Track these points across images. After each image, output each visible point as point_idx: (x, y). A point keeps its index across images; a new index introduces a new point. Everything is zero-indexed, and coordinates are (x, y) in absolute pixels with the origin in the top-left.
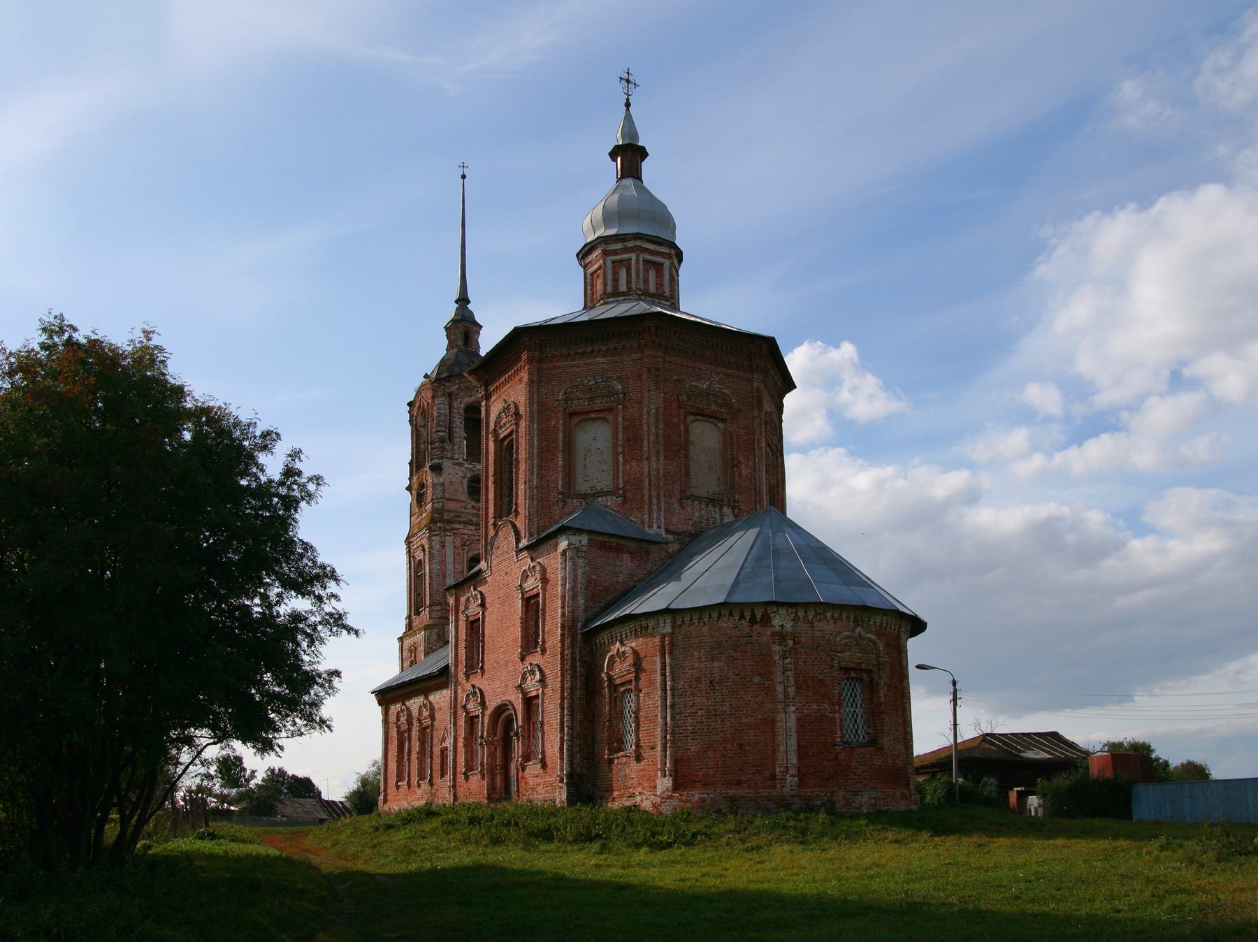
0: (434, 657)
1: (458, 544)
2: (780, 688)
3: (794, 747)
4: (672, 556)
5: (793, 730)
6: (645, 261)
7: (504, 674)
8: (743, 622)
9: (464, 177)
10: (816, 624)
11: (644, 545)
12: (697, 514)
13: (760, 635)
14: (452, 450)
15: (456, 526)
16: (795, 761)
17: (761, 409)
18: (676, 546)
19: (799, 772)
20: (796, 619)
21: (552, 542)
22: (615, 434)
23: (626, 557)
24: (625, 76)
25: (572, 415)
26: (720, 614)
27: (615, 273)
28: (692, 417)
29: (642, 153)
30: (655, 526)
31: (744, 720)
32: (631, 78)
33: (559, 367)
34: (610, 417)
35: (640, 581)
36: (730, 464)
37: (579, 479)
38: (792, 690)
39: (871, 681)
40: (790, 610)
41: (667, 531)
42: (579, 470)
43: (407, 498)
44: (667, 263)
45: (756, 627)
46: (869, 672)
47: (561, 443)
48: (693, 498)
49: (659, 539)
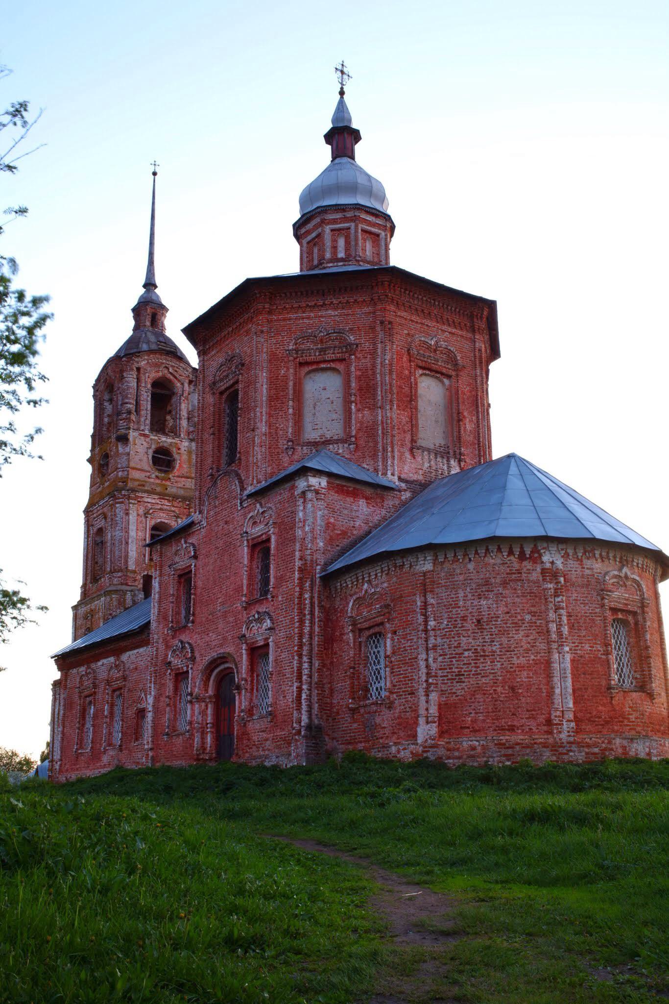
1: (141, 512)
2: (553, 627)
3: (570, 690)
4: (404, 504)
5: (569, 671)
6: (363, 231)
8: (512, 558)
9: (155, 174)
10: (585, 561)
12: (427, 465)
13: (529, 572)
15: (140, 494)
16: (571, 705)
18: (408, 495)
19: (575, 717)
20: (566, 556)
21: (288, 485)
23: (362, 502)
24: (340, 67)
25: (301, 364)
26: (487, 550)
27: (335, 241)
28: (421, 372)
30: (389, 473)
32: (345, 70)
33: (290, 319)
34: (341, 367)
35: (376, 526)
37: (308, 426)
38: (565, 630)
39: (636, 624)
40: (560, 547)
41: (400, 479)
42: (308, 419)
43: (88, 469)
45: (525, 563)
46: (634, 614)
47: (291, 392)
48: (423, 449)
49: (393, 486)
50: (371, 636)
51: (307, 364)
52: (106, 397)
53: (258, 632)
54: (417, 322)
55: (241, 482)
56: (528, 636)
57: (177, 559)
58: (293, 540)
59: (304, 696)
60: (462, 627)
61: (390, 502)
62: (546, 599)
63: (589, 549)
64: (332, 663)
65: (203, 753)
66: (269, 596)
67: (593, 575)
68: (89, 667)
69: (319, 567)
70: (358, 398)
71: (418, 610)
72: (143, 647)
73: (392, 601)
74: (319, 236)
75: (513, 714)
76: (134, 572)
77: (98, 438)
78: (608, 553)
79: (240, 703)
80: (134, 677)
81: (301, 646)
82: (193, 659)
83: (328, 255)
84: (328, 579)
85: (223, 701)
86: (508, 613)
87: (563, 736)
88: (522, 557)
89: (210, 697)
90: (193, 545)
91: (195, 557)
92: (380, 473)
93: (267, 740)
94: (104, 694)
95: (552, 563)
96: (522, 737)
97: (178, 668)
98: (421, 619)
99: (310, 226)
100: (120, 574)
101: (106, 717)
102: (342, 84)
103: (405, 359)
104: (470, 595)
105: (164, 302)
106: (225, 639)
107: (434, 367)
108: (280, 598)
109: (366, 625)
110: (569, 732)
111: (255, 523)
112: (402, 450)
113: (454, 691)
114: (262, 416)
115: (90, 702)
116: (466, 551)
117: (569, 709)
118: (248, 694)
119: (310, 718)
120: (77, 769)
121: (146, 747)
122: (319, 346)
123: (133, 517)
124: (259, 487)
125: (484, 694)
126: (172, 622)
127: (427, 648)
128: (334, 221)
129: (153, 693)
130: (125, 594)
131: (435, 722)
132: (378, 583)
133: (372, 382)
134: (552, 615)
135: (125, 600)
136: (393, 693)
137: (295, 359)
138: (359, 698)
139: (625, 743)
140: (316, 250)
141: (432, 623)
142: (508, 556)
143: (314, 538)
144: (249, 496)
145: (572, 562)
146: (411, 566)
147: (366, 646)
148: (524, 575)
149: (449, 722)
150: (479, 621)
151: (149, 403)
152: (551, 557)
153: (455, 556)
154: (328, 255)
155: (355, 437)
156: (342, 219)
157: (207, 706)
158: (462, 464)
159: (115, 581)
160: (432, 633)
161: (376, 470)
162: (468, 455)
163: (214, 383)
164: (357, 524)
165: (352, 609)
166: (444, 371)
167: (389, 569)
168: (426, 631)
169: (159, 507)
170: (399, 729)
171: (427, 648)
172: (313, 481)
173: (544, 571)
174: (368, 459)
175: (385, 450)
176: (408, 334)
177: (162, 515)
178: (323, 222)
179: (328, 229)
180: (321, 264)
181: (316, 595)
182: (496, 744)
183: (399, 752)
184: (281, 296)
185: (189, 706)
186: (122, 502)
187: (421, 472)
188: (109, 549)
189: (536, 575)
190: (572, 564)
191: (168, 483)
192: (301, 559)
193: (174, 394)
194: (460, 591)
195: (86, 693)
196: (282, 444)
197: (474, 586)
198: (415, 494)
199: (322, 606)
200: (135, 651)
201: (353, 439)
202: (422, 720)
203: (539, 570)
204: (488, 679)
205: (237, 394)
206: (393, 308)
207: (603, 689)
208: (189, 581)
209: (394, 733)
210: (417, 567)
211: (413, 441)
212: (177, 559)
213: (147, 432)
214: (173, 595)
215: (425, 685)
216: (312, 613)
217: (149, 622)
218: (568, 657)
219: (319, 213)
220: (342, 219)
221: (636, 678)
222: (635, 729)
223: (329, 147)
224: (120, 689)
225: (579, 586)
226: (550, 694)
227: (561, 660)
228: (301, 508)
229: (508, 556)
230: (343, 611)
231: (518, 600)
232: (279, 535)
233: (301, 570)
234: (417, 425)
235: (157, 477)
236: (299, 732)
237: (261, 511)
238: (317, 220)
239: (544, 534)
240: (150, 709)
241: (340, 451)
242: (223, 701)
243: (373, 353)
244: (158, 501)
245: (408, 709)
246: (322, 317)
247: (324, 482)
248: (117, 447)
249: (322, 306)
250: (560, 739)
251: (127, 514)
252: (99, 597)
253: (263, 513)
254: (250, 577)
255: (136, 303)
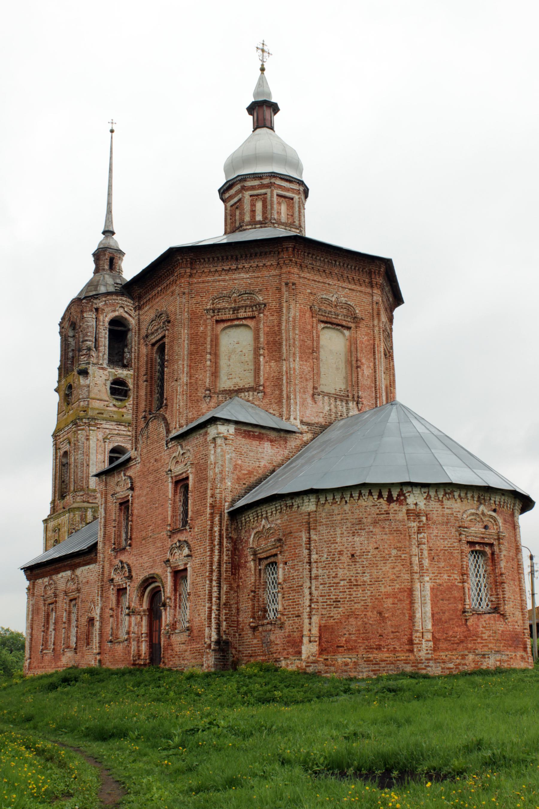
0: (76, 537)
1: (100, 437)
2: (415, 560)
3: (429, 614)
4: (306, 444)
6: (278, 195)
7: (152, 550)
9: (112, 131)
10: (445, 502)
11: (282, 434)
12: (327, 408)
14: (98, 357)
15: (99, 422)
16: (430, 627)
17: (379, 320)
19: (433, 637)
20: (428, 498)
21: (202, 431)
22: (257, 338)
23: (267, 445)
24: (261, 46)
25: (218, 322)
26: (360, 494)
27: (253, 205)
28: (323, 325)
29: (275, 108)
31: (383, 589)
32: (266, 48)
33: (208, 282)
35: (279, 465)
36: (353, 365)
38: (426, 562)
39: (493, 554)
41: (302, 422)
43: (56, 397)
44: (296, 197)
45: (393, 505)
46: (491, 545)
50: (268, 565)
51: (223, 321)
52: (71, 334)
53: (179, 559)
54: (319, 282)
55: (167, 425)
56: (394, 568)
57: (118, 489)
58: (206, 479)
59: (213, 615)
60: (339, 560)
61: (293, 443)
62: (410, 536)
63: (449, 491)
64: (238, 586)
65: (139, 659)
66: (187, 528)
67: (452, 514)
68: (51, 579)
69: (227, 504)
70: (266, 351)
71: (304, 545)
72: (92, 563)
73: (284, 535)
74: (240, 200)
75: (380, 636)
76: (95, 491)
77: (65, 369)
78: (466, 494)
79: (166, 618)
80: (85, 590)
81: (211, 571)
82: (130, 577)
83: (247, 218)
84: (235, 515)
85: (154, 614)
86: (377, 548)
87: (423, 654)
88: (390, 499)
89: (144, 611)
90: (130, 477)
91: (132, 488)
92: (284, 418)
93: (186, 651)
94: (62, 603)
95: (416, 504)
96: (387, 655)
97: (119, 585)
98: (306, 552)
99: (232, 192)
100: (81, 493)
101: (65, 623)
102: (263, 61)
103: (307, 315)
104: (345, 533)
105: (121, 248)
106: (154, 561)
107: (335, 321)
108: (196, 530)
109: (264, 555)
110: (427, 650)
111: (177, 462)
112: (304, 396)
113: (332, 615)
114: (184, 368)
115: (52, 610)
116: (342, 495)
117: (428, 631)
118: (172, 611)
119: (218, 633)
120: (43, 667)
121: (95, 651)
122: (233, 305)
123: (93, 443)
124: (181, 431)
125: (356, 618)
126: (114, 544)
127: (311, 577)
128: (253, 188)
129: (100, 605)
130: (86, 511)
131: (316, 642)
132: (273, 520)
133: (278, 337)
134: (415, 550)
135: (86, 516)
136: (284, 615)
137: (212, 317)
138: (258, 617)
139: (477, 658)
140: (238, 213)
141: (314, 557)
142: (378, 499)
143: (223, 479)
144: (172, 439)
145: (433, 503)
146: (298, 507)
147: (265, 573)
148: (391, 515)
149: (327, 642)
150: (353, 555)
151: (107, 339)
152: (415, 499)
153: (334, 499)
154: (247, 218)
155: (263, 385)
156: (259, 189)
157: (141, 618)
158: (360, 405)
159: (78, 499)
160: (314, 565)
161: (281, 416)
162: (365, 397)
163: (147, 336)
164: (262, 464)
165: (253, 541)
166: (344, 323)
167: (281, 509)
168: (310, 563)
169: (116, 432)
170: (288, 646)
171: (311, 577)
172: (223, 429)
173: (408, 511)
174: (274, 406)
175: (288, 398)
176: (311, 293)
177: (119, 439)
178: (244, 188)
179: (247, 194)
180: (241, 227)
181: (224, 528)
182: (365, 661)
183: (287, 665)
184: (200, 261)
185: (127, 618)
186: (83, 429)
187: (321, 415)
188: (72, 470)
189: (402, 515)
190: (434, 505)
191: (124, 410)
192: (212, 497)
193: (129, 330)
194: (338, 529)
195: (49, 601)
196: (201, 393)
197: (349, 525)
198: (316, 435)
199: (230, 537)
200: (87, 567)
201: (261, 388)
202: (305, 640)
203: (404, 511)
204: (359, 605)
205: (165, 347)
206: (296, 270)
207: (459, 613)
208: (127, 508)
209: (284, 649)
210: (303, 508)
211: (315, 388)
212: (118, 489)
213: (105, 366)
214: (115, 520)
215: (308, 609)
216: (221, 544)
217: (97, 543)
218: (428, 586)
219: (240, 181)
220: (259, 189)
221: (492, 601)
222: (487, 646)
223: (251, 117)
224: (75, 599)
225: (439, 524)
226: (412, 618)
227: (422, 589)
228: (212, 452)
229: (378, 499)
230: (247, 542)
231: (385, 537)
232: (196, 474)
233: (212, 506)
234: (319, 374)
235: (114, 405)
236: (210, 646)
237: (182, 452)
238: (238, 187)
239: (408, 481)
240: (98, 619)
241: (251, 399)
242: (154, 614)
243: (279, 311)
244: (115, 427)
245: (295, 630)
246: (235, 279)
247: (232, 429)
248: (79, 380)
249: (235, 270)
250: (420, 657)
251: (88, 439)
252: (64, 513)
253: (183, 454)
254: (174, 510)
255: (96, 248)
